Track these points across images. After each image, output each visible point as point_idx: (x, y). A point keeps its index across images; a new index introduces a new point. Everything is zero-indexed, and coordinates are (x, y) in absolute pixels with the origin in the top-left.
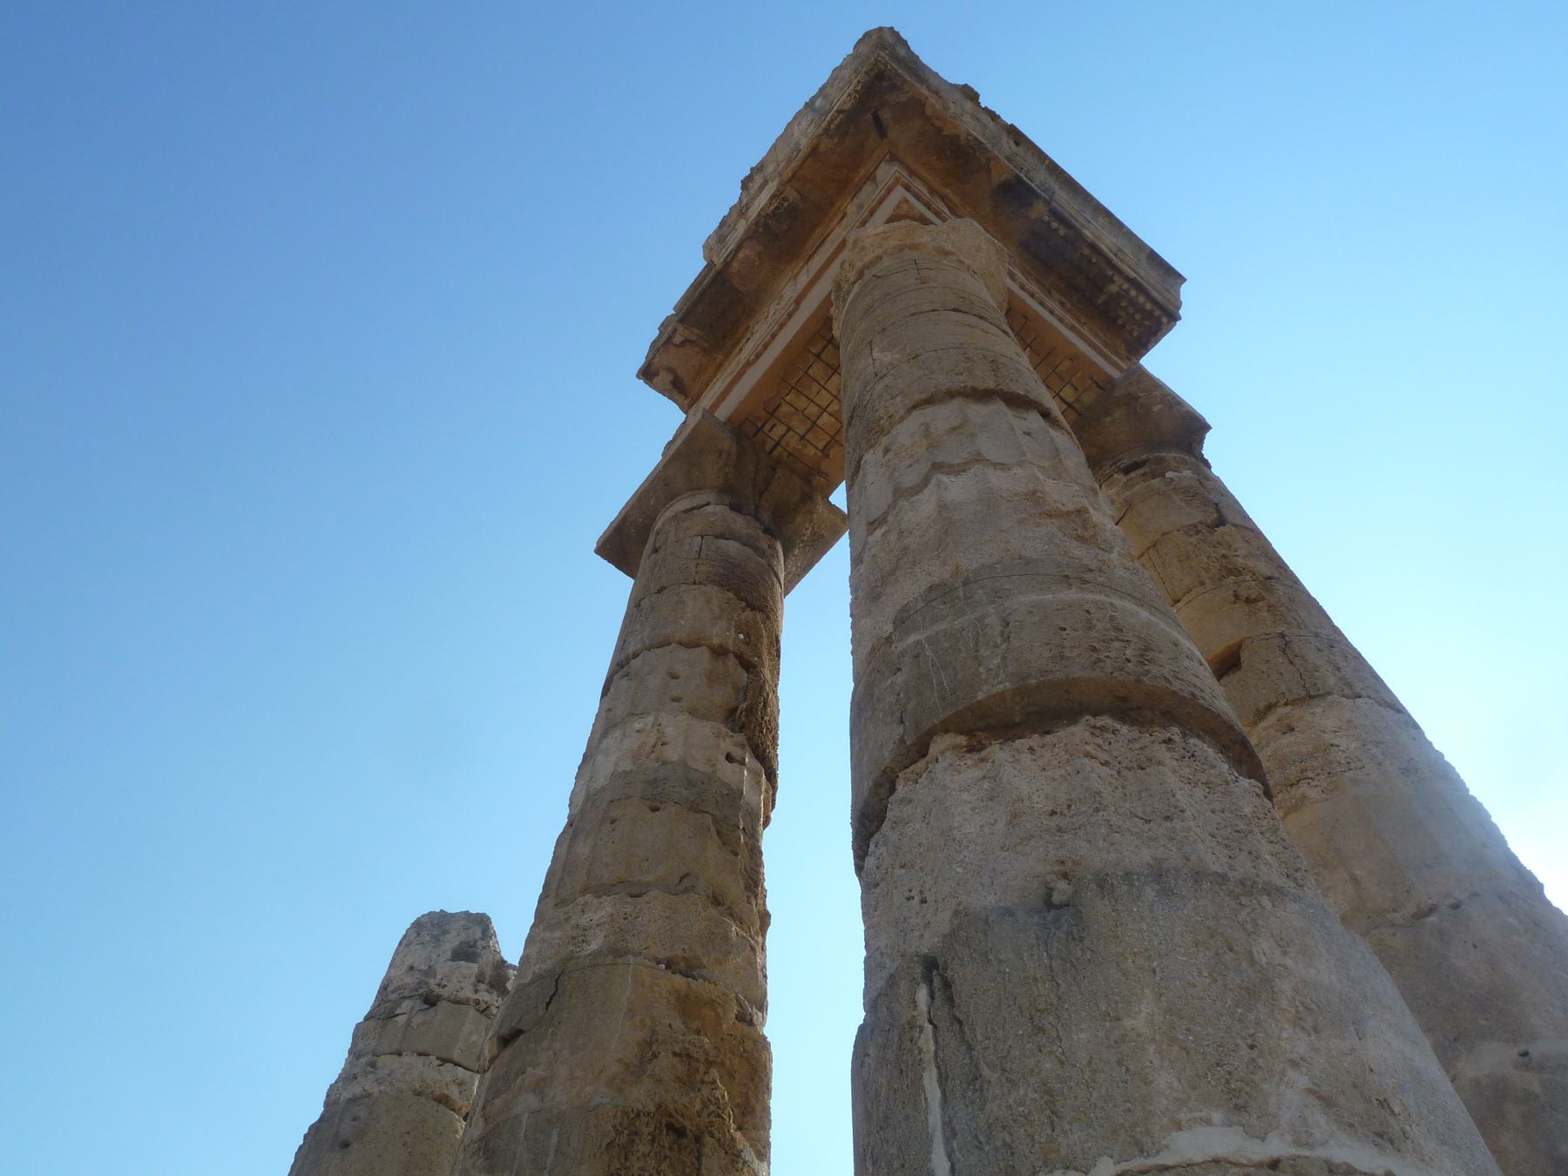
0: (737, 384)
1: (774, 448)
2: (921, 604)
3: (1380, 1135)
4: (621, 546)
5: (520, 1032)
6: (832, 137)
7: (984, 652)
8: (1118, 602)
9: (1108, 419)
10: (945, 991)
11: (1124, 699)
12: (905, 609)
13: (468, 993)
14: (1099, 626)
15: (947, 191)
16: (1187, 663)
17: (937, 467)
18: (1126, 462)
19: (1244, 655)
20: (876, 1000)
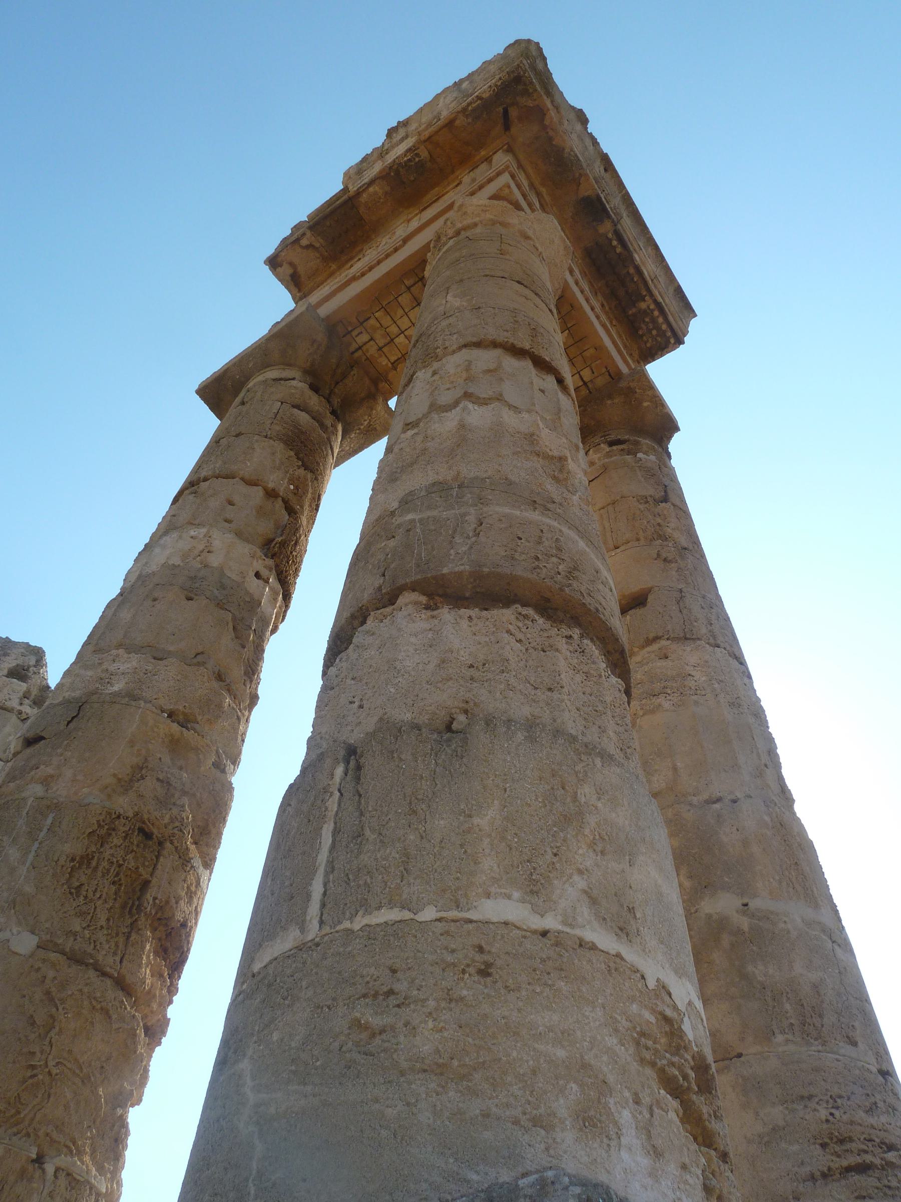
0: (338, 295)
1: (357, 350)
2: (423, 493)
3: (621, 929)
4: (218, 392)
5: (42, 738)
6: (467, 117)
7: (458, 539)
8: (565, 530)
9: (609, 402)
10: (356, 771)
11: (548, 600)
12: (411, 493)
13: (14, 703)
14: (547, 543)
15: (543, 190)
16: (601, 587)
17: (467, 395)
18: (613, 437)
19: (650, 598)
20: (307, 768)
